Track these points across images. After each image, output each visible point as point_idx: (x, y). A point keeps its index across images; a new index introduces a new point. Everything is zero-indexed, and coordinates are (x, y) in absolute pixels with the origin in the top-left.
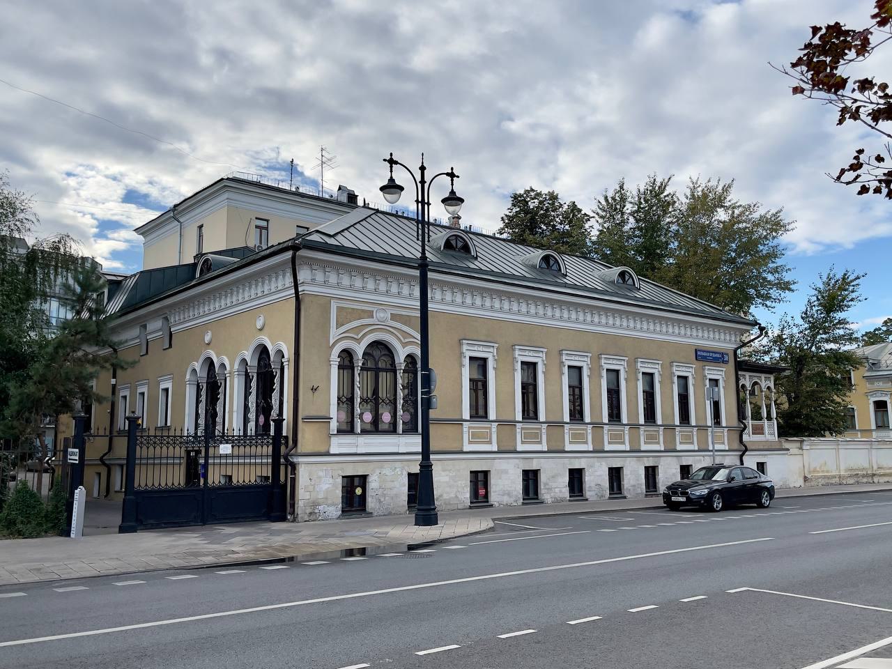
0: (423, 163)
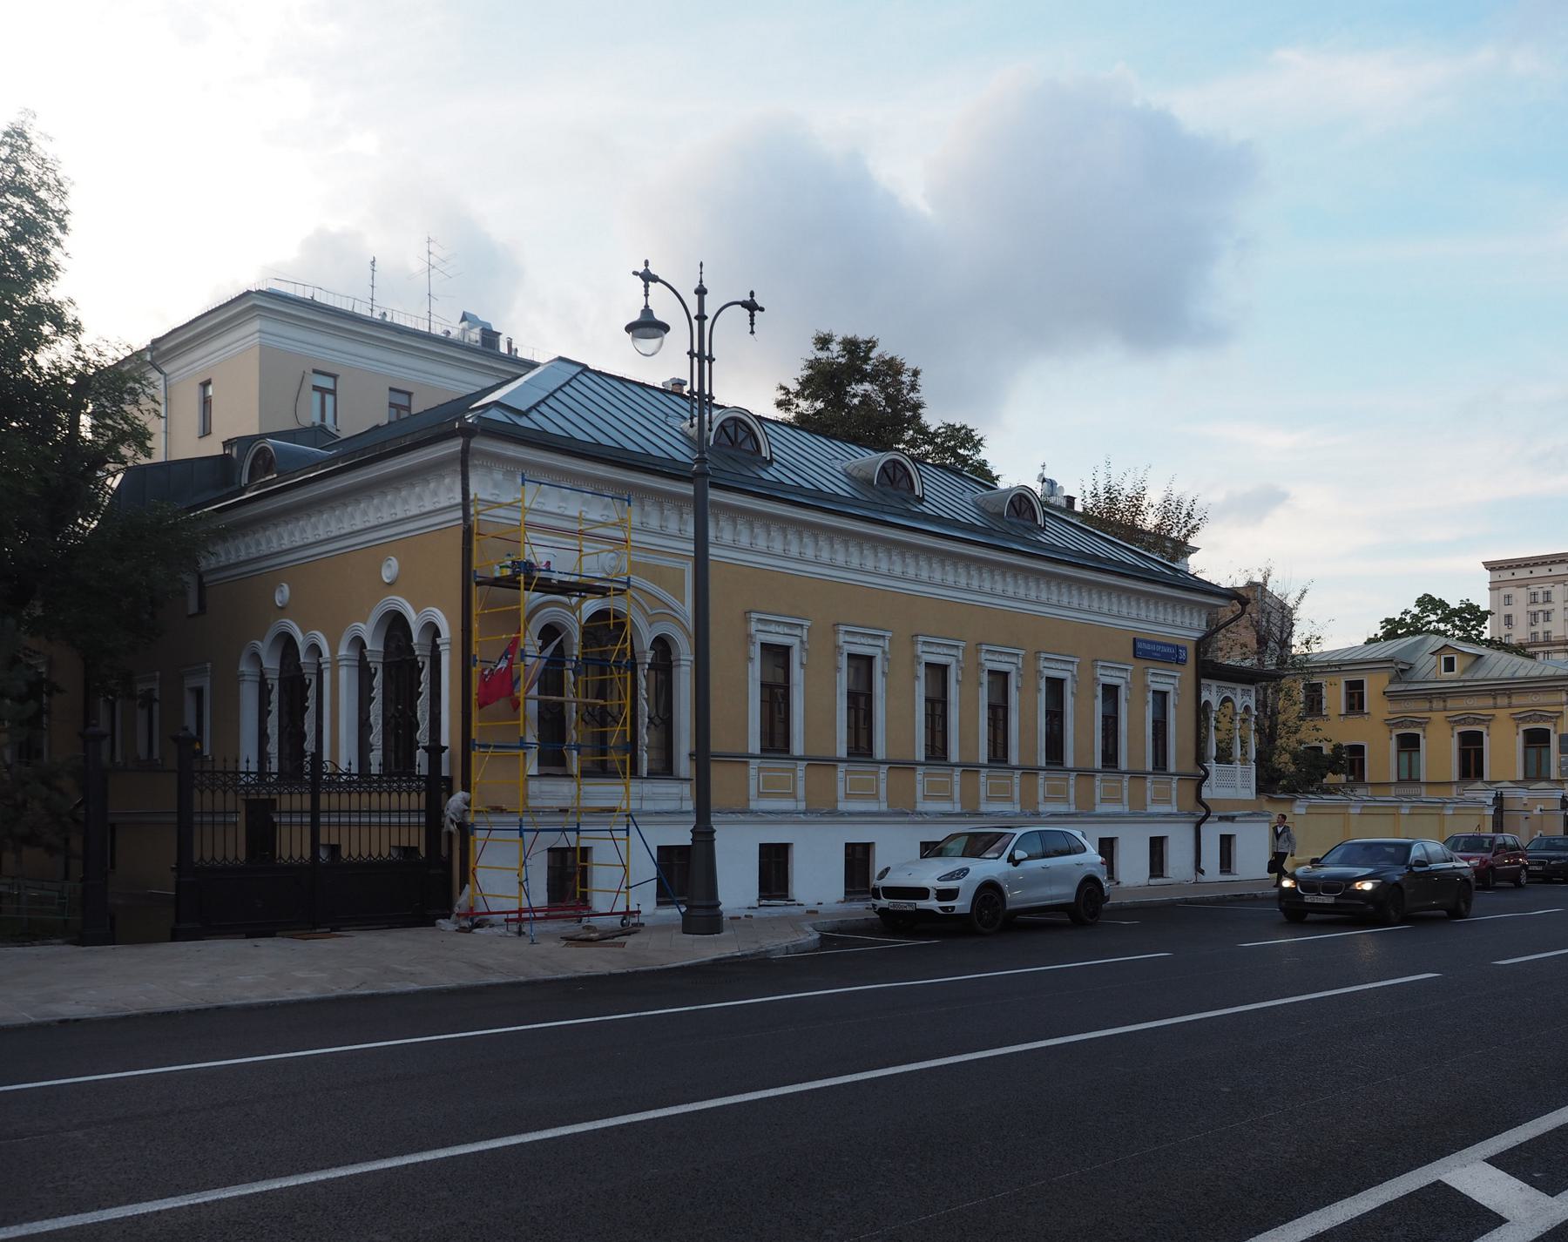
0: (701, 281)
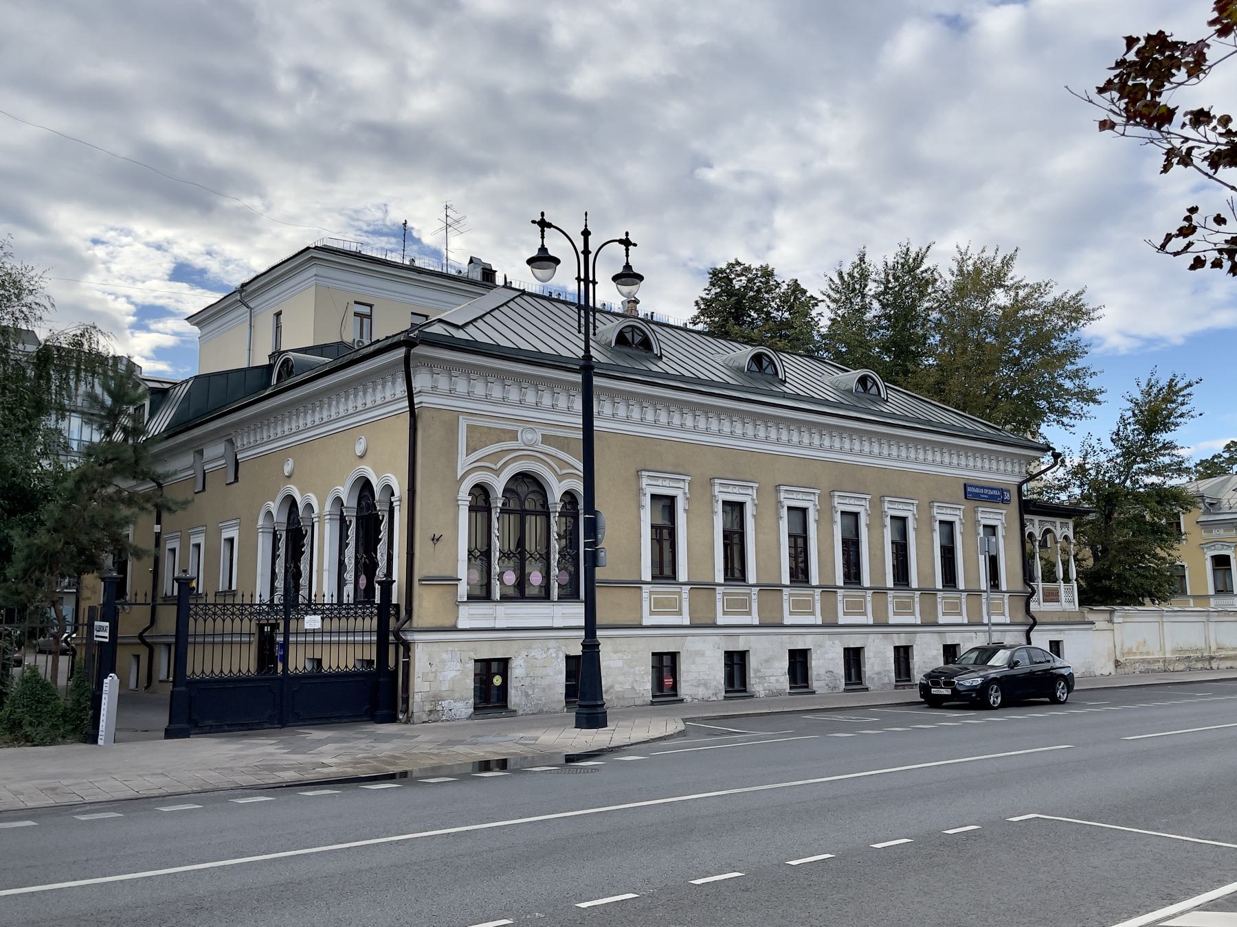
0: (586, 226)
